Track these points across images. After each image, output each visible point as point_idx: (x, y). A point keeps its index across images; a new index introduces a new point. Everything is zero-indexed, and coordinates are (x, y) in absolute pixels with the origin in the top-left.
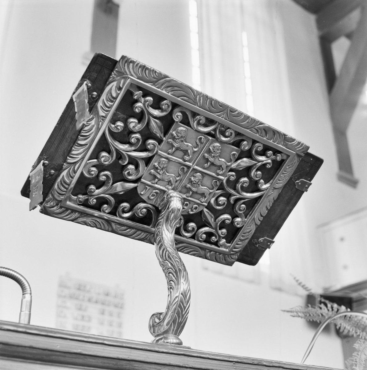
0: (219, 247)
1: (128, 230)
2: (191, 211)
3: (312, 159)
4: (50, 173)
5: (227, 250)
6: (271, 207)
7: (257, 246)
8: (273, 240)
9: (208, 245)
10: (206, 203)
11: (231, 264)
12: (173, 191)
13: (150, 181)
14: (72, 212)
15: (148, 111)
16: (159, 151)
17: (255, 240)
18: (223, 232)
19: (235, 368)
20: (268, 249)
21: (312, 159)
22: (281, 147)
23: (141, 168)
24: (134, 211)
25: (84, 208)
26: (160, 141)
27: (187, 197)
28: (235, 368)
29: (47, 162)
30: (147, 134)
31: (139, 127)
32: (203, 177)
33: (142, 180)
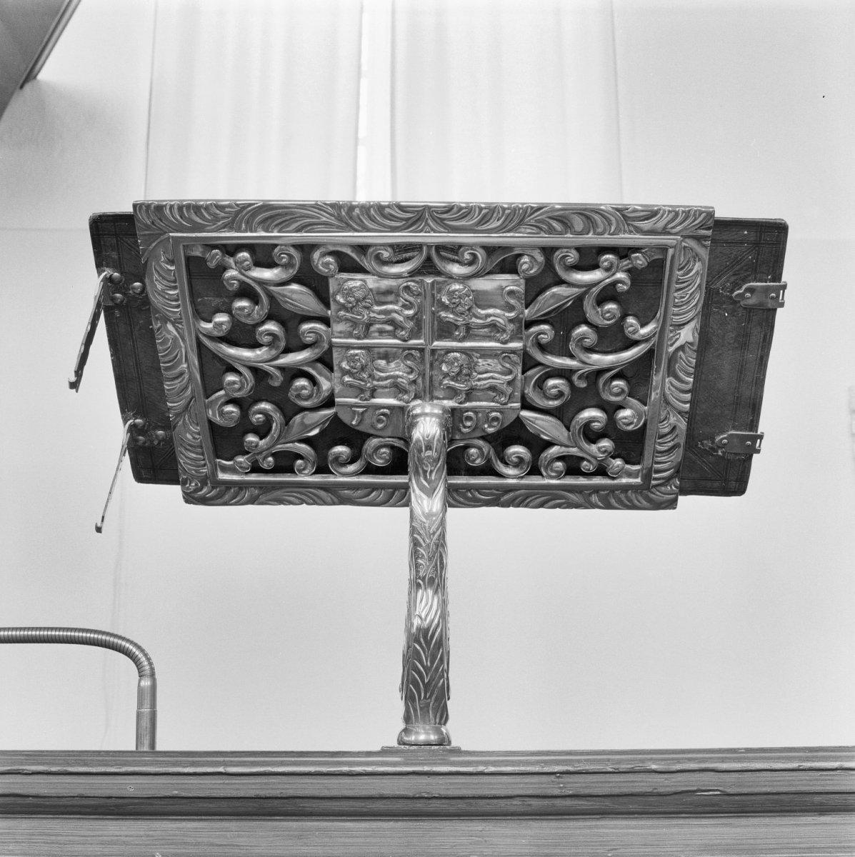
0: (614, 479)
1: (373, 495)
2: (489, 427)
3: (746, 232)
4: (157, 436)
5: (639, 480)
6: (696, 367)
7: (720, 453)
8: (759, 433)
9: (582, 481)
10: (517, 403)
11: (672, 504)
12: (418, 402)
13: (356, 397)
14: (241, 489)
15: (254, 280)
16: (334, 340)
17: (705, 442)
18: (601, 447)
19: (562, 785)
20: (755, 456)
21: (746, 232)
22: (626, 239)
23: (322, 380)
24: (364, 456)
25: (259, 476)
26: (326, 321)
27: (460, 403)
28: (562, 785)
29: (138, 421)
30: (289, 319)
31: (258, 312)
32: (470, 356)
33: (337, 400)
